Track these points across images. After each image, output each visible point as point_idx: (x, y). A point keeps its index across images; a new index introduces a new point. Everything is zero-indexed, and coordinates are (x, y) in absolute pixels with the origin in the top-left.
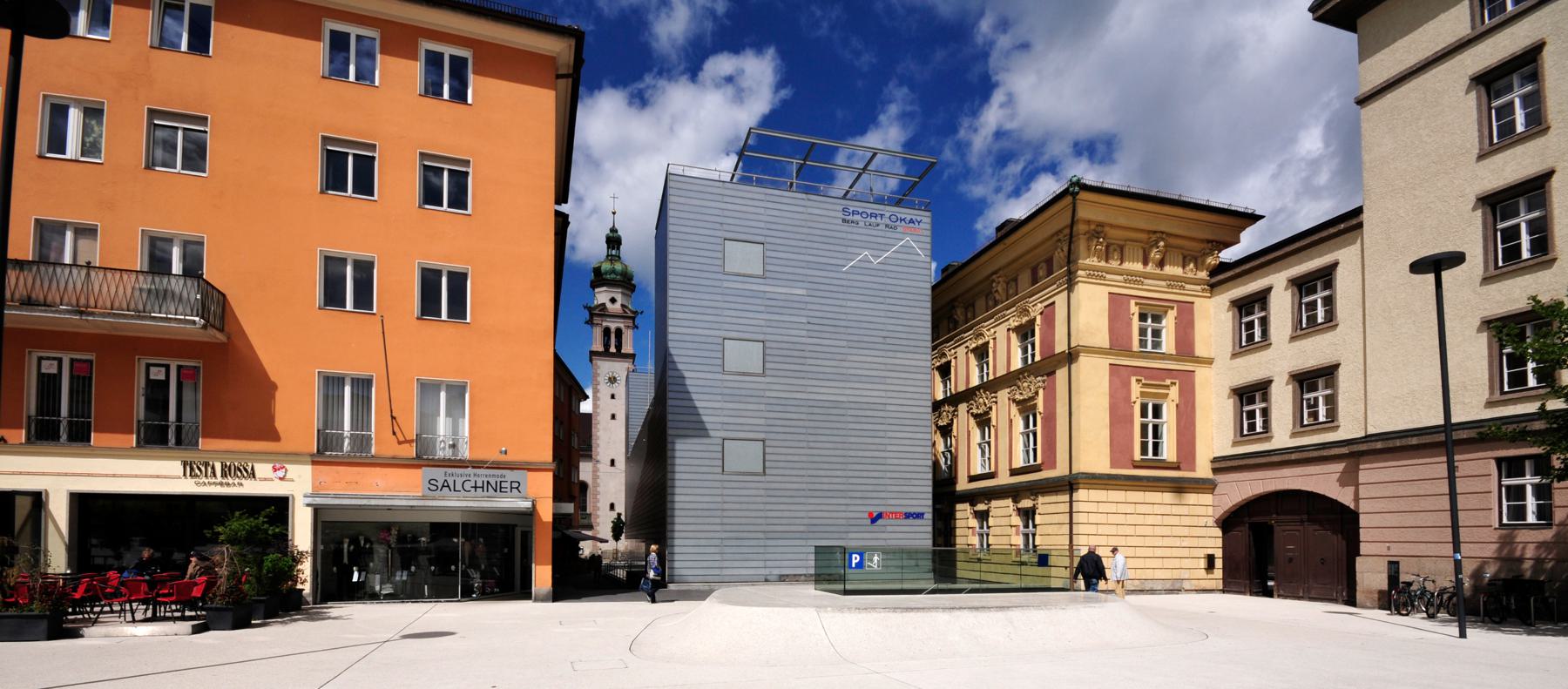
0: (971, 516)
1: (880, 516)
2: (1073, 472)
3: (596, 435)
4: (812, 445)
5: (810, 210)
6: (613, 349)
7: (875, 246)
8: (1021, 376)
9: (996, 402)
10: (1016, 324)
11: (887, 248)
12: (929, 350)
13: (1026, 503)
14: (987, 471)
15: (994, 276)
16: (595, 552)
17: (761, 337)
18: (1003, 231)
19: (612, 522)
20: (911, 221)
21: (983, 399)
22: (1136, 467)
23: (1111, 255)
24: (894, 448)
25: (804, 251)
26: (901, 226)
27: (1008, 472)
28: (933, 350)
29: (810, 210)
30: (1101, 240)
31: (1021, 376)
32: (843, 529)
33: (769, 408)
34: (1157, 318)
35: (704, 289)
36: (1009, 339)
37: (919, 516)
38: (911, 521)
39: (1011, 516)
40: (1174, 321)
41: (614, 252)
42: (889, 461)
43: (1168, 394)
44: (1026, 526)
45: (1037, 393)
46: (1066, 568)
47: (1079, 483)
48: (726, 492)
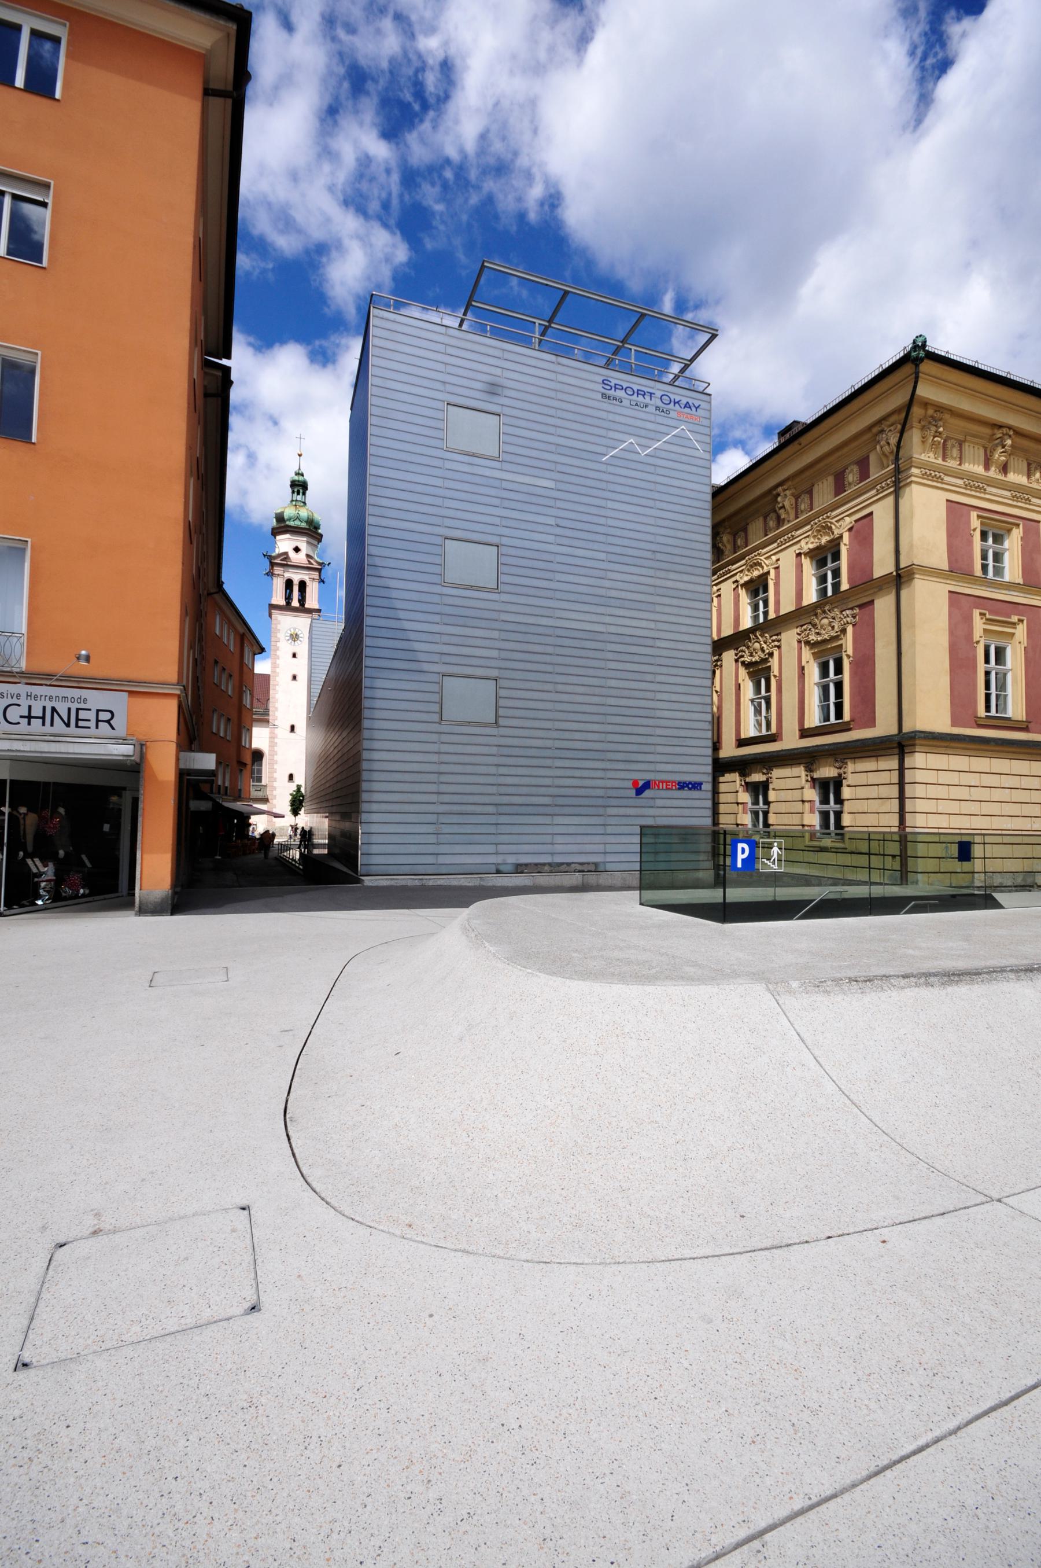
0: (741, 789)
1: (647, 785)
2: (905, 730)
3: (274, 698)
4: (560, 688)
5: (560, 378)
6: (295, 603)
7: (643, 433)
8: (819, 611)
9: (779, 647)
10: (811, 546)
11: (658, 436)
12: (709, 573)
13: (827, 772)
14: (764, 732)
15: (780, 489)
16: (269, 828)
17: (495, 540)
18: (787, 436)
19: (291, 795)
20: (687, 405)
21: (759, 645)
22: (981, 726)
23: (948, 452)
24: (665, 697)
25: (552, 430)
26: (675, 411)
27: (797, 732)
28: (714, 575)
29: (560, 378)
30: (941, 429)
31: (819, 611)
32: (600, 802)
33: (504, 635)
34: (998, 539)
35: (419, 469)
36: (799, 567)
37: (696, 786)
38: (686, 793)
39: (802, 788)
40: (1020, 543)
41: (299, 498)
42: (659, 714)
43: (1013, 634)
44: (756, 802)
45: (844, 631)
46: (894, 856)
47: (914, 745)
48: (445, 748)
